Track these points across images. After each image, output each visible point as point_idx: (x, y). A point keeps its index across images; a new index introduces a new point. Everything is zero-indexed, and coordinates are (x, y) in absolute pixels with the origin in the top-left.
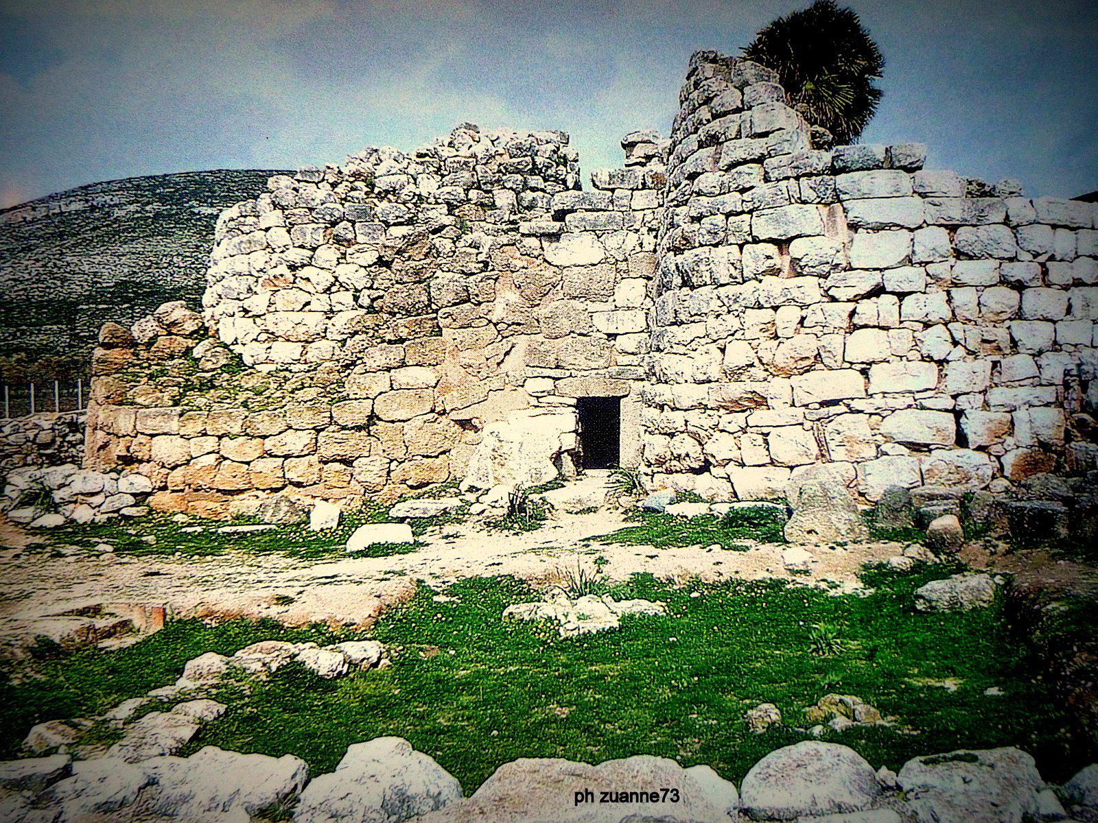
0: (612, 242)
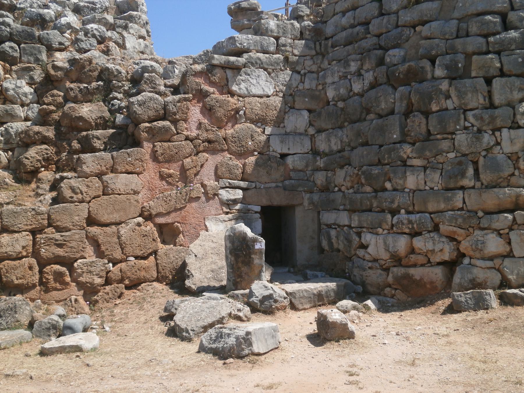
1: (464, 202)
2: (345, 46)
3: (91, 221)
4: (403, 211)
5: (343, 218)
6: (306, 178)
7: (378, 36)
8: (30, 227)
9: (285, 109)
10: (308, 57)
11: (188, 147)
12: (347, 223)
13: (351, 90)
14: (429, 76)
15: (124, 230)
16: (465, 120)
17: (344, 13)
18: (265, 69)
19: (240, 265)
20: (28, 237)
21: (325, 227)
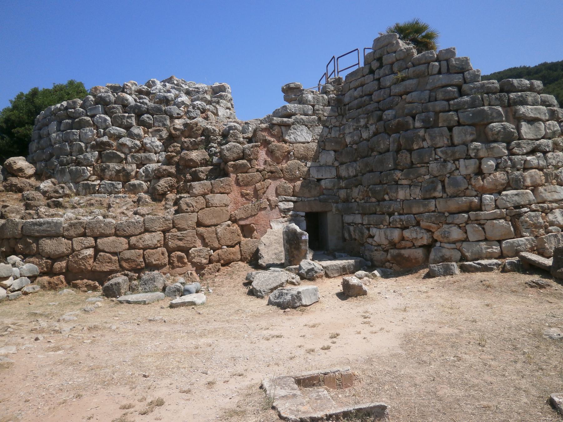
1: (436, 207)
3: (199, 224)
4: (396, 213)
5: (358, 219)
6: (333, 194)
7: (378, 102)
8: (162, 229)
10: (333, 117)
11: (258, 176)
12: (360, 222)
13: (361, 137)
14: (412, 127)
15: (219, 229)
16: (436, 154)
17: (356, 89)
18: (306, 126)
19: (293, 250)
21: (346, 225)
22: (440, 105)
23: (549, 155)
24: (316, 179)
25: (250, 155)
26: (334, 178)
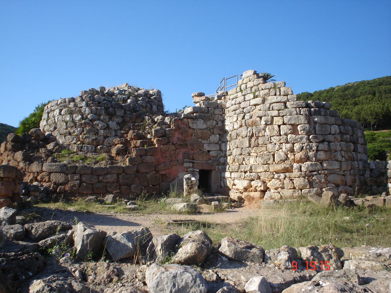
0: (209, 123)
2: (232, 111)
6: (217, 160)
7: (244, 108)
9: (210, 133)
10: (219, 115)
11: (173, 147)
16: (271, 140)
17: (233, 99)
20: (116, 176)
21: (223, 178)
22: (275, 113)
23: (331, 144)
24: (207, 150)
25: (169, 135)
26: (218, 150)
